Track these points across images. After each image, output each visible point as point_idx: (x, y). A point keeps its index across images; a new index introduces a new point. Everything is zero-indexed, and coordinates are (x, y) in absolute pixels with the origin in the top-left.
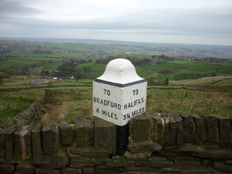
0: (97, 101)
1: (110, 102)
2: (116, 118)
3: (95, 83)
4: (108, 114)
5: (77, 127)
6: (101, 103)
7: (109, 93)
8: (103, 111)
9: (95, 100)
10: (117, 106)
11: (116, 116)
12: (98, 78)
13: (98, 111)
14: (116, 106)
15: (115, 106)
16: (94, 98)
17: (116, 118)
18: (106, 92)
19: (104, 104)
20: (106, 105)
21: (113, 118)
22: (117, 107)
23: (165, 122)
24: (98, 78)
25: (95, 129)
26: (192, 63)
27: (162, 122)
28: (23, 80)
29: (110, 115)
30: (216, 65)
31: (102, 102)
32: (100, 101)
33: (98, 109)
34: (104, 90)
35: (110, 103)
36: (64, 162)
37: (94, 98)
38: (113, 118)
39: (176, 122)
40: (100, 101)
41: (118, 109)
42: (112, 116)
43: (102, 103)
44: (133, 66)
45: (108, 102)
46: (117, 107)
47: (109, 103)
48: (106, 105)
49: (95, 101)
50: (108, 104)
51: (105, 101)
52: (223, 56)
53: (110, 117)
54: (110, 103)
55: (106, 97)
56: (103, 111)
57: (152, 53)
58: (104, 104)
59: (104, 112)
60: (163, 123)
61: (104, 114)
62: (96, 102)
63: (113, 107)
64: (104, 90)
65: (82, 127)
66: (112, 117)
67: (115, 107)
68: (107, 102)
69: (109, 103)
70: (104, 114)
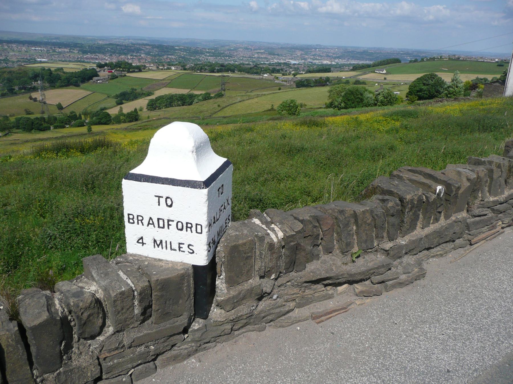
0: (138, 220)
1: (173, 221)
2: (192, 251)
3: (126, 184)
4: (169, 246)
5: (111, 292)
6: (149, 224)
7: (169, 202)
8: (155, 241)
9: (133, 219)
10: (192, 226)
11: (190, 247)
12: (136, 171)
13: (141, 241)
14: (191, 228)
15: (187, 227)
16: (129, 215)
17: (192, 251)
18: (162, 200)
19: (159, 227)
20: (163, 227)
21: (184, 252)
22: (194, 229)
23: (277, 237)
24: (136, 171)
25: (153, 285)
26: (179, 75)
27: (273, 240)
28: (105, 275)
29: (175, 246)
30: (219, 76)
31: (151, 222)
32: (146, 222)
33: (142, 238)
34: (156, 196)
35: (175, 223)
36: (89, 374)
37: (129, 215)
38: (184, 252)
39: (296, 232)
40: (146, 222)
41: (197, 232)
42: (180, 248)
43: (153, 224)
44: (202, 130)
45: (169, 221)
46: (194, 229)
47: (170, 223)
48: (163, 227)
49: (131, 221)
50: (169, 225)
51: (158, 219)
52: (231, 61)
53: (175, 250)
54: (174, 224)
55: (165, 213)
56: (155, 241)
57: (96, 59)
58: (156, 225)
59: (158, 242)
60: (275, 240)
61: (158, 246)
62: (134, 223)
63: (182, 230)
64: (156, 196)
65: (123, 289)
66: (180, 250)
67: (189, 229)
68: (166, 222)
69: (170, 223)
70: (158, 246)
